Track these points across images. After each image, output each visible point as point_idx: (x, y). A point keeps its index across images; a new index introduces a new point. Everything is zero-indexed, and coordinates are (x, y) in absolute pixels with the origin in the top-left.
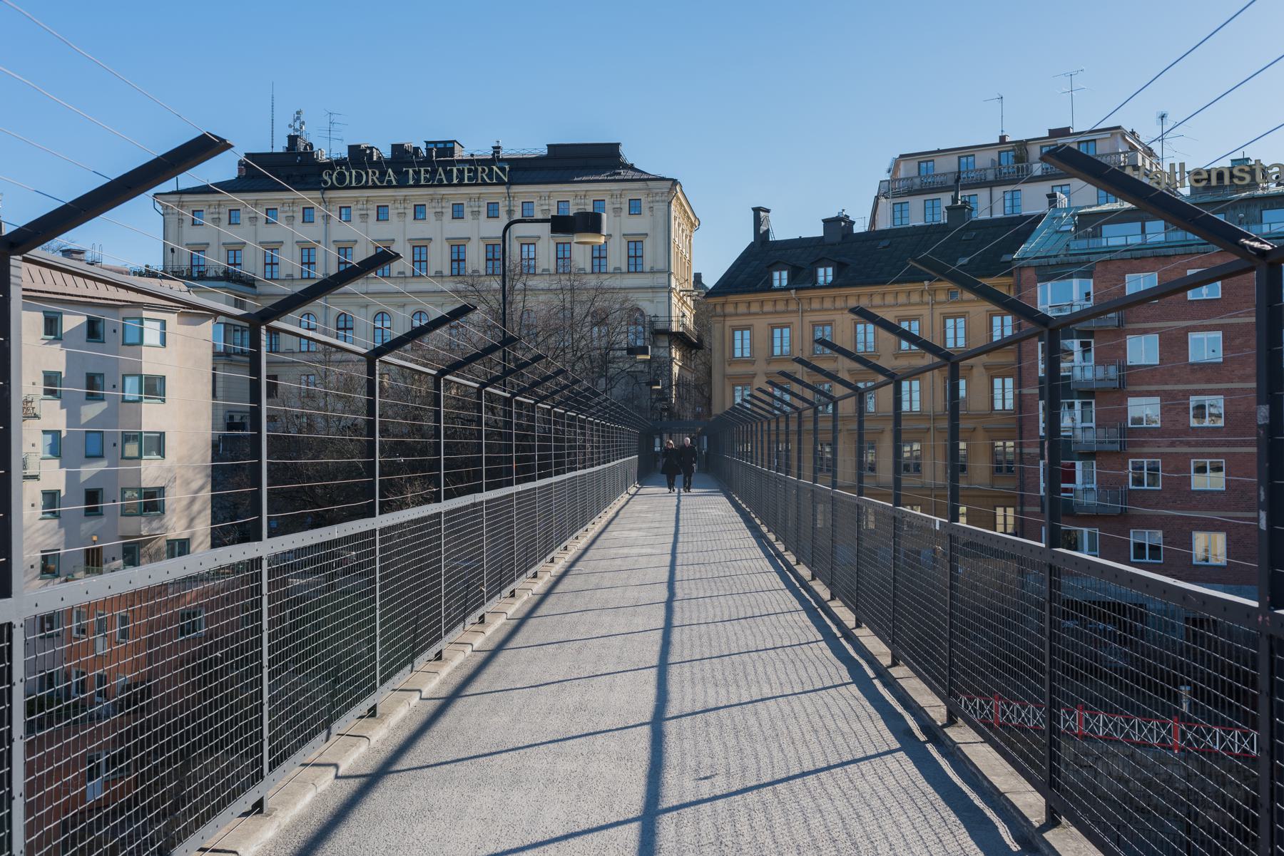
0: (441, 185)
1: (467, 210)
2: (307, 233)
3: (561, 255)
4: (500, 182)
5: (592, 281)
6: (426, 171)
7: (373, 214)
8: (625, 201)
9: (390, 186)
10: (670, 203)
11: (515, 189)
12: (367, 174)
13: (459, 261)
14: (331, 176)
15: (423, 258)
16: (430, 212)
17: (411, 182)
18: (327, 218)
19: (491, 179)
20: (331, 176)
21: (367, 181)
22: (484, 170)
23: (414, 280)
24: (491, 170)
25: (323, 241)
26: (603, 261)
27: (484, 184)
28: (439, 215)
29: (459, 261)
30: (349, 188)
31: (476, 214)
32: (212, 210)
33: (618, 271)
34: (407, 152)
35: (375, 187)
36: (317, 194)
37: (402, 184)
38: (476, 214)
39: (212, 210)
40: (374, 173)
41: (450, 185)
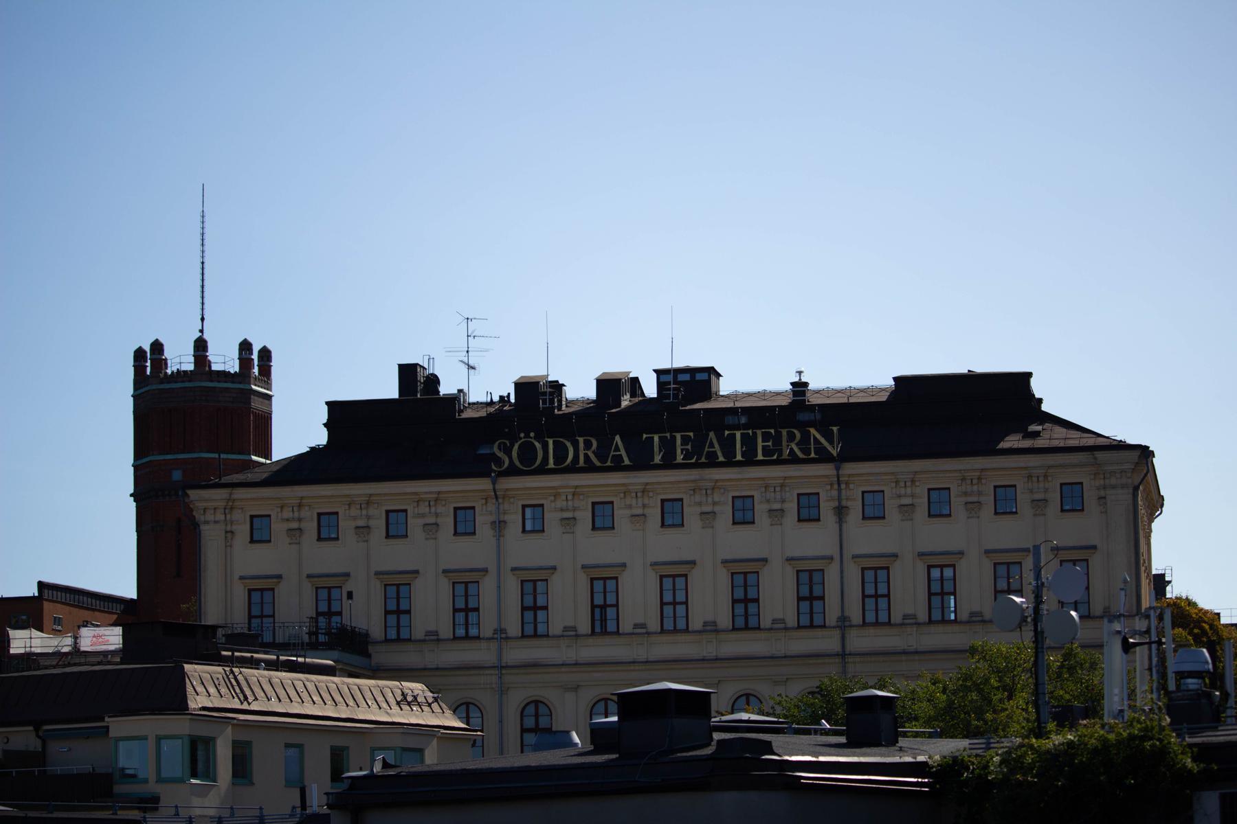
0: (712, 463)
1: (760, 508)
2: (814, 541)
3: (256, 612)
4: (824, 457)
5: (518, 653)
6: (685, 440)
7: (585, 516)
8: (922, 491)
9: (618, 467)
10: (1136, 489)
11: (850, 468)
12: (576, 445)
13: (398, 612)
14: (508, 452)
15: (882, 590)
16: (691, 512)
17: (657, 459)
18: (499, 526)
19: (806, 451)
20: (508, 452)
21: (576, 457)
22: (791, 437)
23: (665, 638)
24: (806, 437)
25: (492, 569)
26: (541, 615)
27: (794, 460)
28: (708, 517)
29: (746, 601)
30: (543, 470)
31: (777, 515)
32: (287, 514)
33: (571, 633)
34: (248, 408)
35: (590, 468)
36: (483, 484)
37: (642, 463)
38: (777, 515)
39: (287, 514)
40: (588, 445)
41: (730, 463)
